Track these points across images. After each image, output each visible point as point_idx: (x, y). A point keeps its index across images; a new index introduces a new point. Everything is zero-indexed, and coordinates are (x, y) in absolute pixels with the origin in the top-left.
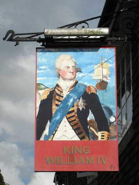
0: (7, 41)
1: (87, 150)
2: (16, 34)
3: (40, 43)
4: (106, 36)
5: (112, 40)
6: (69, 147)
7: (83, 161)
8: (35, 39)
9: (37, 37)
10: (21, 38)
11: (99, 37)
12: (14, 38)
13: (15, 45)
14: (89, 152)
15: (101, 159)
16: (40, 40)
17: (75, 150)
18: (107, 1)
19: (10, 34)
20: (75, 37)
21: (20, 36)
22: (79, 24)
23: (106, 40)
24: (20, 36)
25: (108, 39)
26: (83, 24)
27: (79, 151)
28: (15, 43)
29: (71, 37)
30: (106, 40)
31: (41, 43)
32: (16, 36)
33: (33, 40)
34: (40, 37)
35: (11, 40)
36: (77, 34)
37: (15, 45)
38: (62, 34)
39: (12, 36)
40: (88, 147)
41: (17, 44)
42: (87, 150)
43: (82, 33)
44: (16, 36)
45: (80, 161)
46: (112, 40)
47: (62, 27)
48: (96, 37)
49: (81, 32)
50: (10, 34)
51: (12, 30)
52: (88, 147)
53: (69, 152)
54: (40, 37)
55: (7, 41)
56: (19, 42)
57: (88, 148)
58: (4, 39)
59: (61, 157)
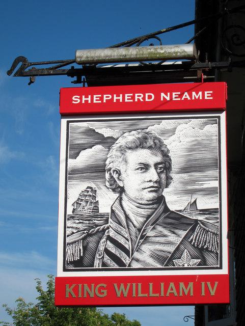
0: (15, 76)
1: (102, 291)
2: (31, 63)
3: (72, 77)
4: (191, 58)
5: (204, 66)
6: (74, 286)
7: (175, 291)
8: (64, 70)
9: (68, 67)
10: (39, 70)
11: (180, 62)
12: (27, 70)
13: (29, 84)
14: (105, 294)
15: (206, 286)
16: (71, 73)
17: (85, 292)
18: (198, 5)
19: (21, 64)
20: (137, 64)
21: (37, 67)
22: (145, 40)
23: (193, 68)
24: (37, 67)
25: (197, 64)
26: (151, 40)
27: (90, 292)
28: (27, 79)
29: (130, 65)
30: (193, 68)
31: (75, 78)
32: (30, 68)
33: (61, 72)
34: (73, 67)
35: (21, 73)
36: (141, 56)
37: (29, 84)
38: (107, 58)
39: (22, 68)
40: (105, 285)
41: (31, 82)
42: (102, 291)
43: (132, 57)
44: (30, 68)
45: (169, 291)
46: (206, 67)
47: (118, 46)
48: (176, 63)
49: (142, 54)
50: (21, 64)
51: (23, 57)
52: (105, 285)
53: (74, 296)
54: (73, 67)
55: (15, 76)
56: (36, 77)
57: (102, 288)
58: (9, 73)
59: (140, 285)
